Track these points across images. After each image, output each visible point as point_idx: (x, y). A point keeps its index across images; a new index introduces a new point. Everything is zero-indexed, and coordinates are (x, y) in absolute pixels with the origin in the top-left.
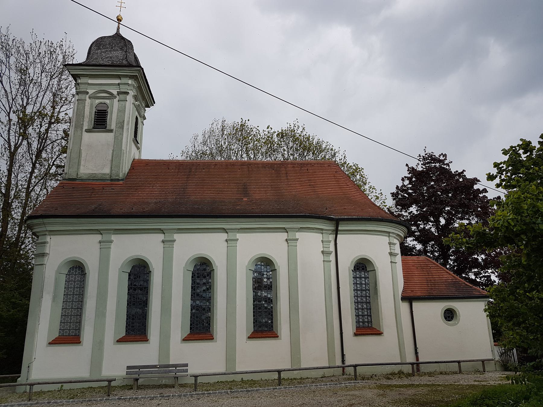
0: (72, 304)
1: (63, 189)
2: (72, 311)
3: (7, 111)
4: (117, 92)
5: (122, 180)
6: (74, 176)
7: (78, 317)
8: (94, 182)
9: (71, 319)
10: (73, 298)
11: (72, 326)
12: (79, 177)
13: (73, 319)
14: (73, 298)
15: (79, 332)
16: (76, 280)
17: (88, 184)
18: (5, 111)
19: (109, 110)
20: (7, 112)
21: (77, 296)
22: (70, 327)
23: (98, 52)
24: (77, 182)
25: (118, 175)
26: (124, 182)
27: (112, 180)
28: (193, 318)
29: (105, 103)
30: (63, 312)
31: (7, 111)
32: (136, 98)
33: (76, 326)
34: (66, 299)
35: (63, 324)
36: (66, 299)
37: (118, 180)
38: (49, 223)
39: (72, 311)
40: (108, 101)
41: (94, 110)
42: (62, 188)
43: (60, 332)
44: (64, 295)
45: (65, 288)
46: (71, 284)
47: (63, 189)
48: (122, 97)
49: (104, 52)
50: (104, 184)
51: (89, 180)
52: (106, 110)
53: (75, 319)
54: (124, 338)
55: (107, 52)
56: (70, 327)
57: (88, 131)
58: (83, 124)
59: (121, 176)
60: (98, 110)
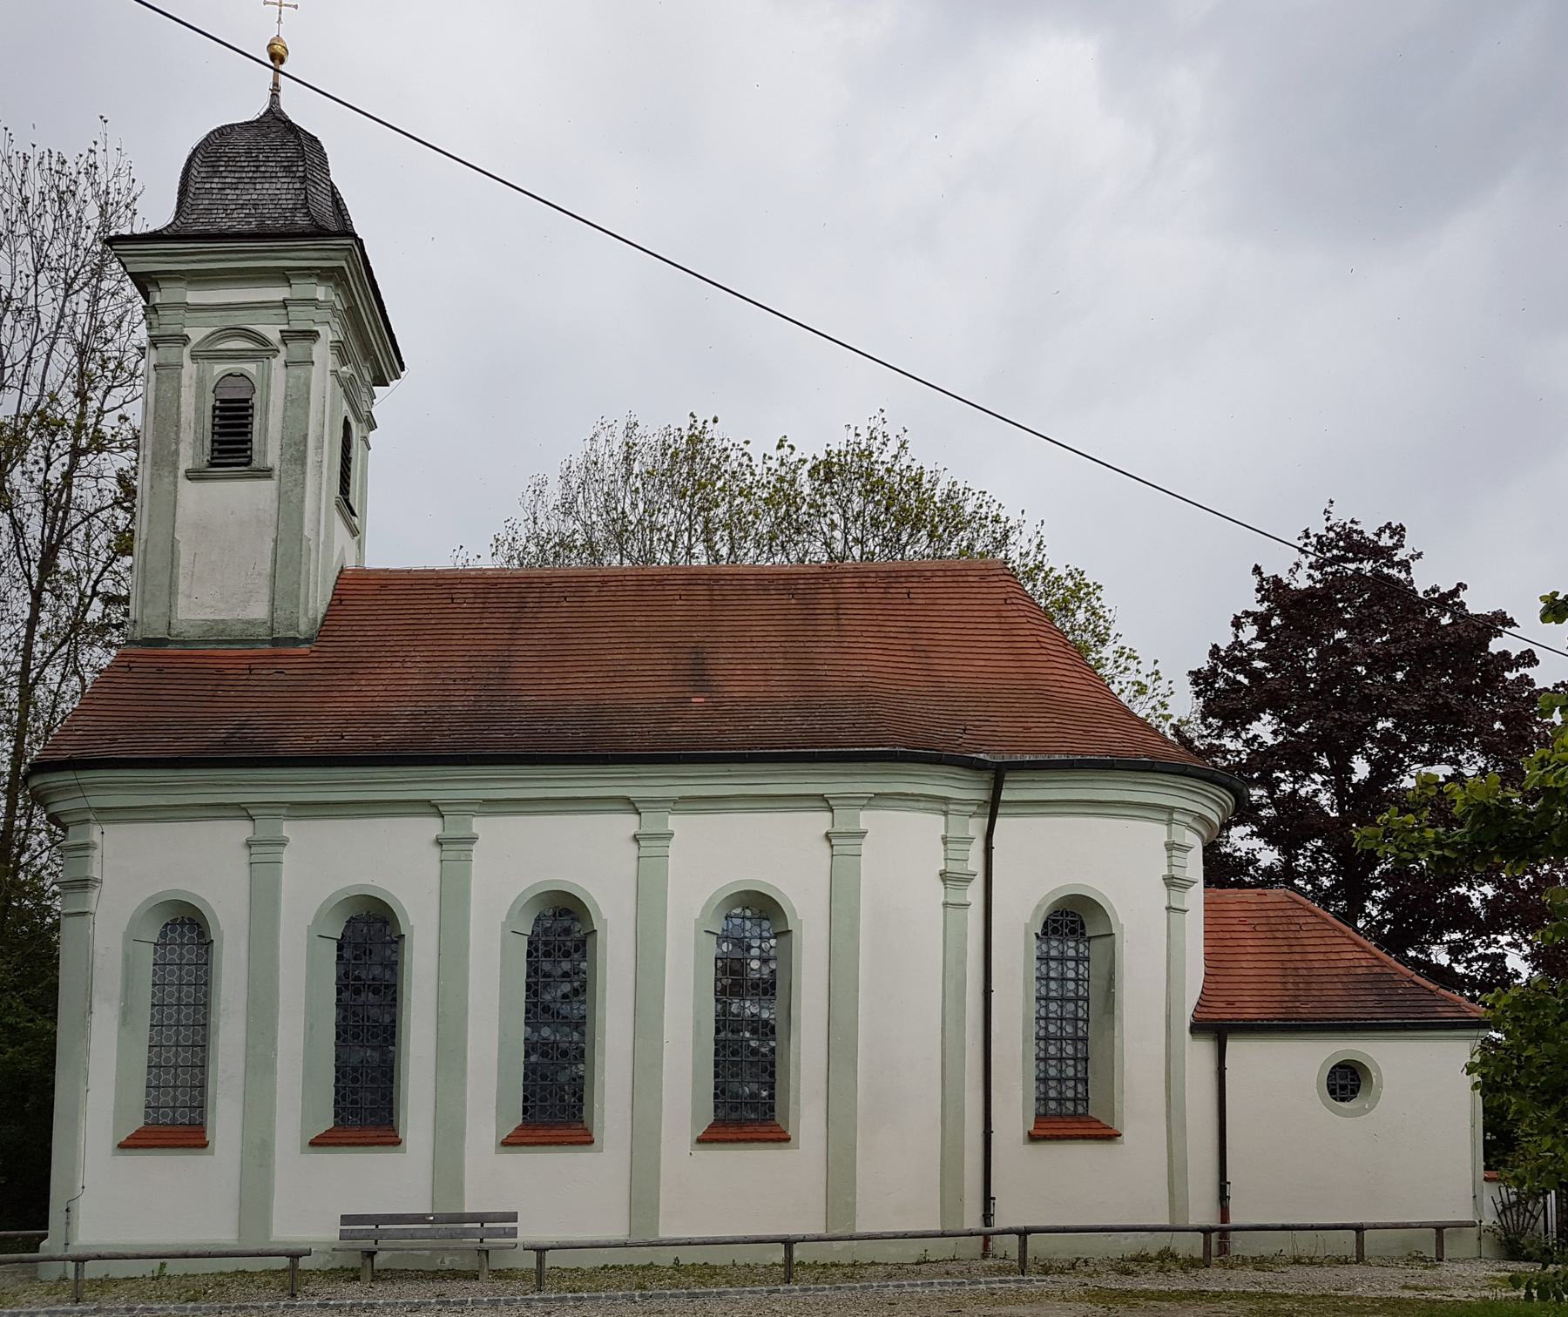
2: (177, 1054)
5: (307, 641)
6: (161, 633)
7: (197, 1071)
9: (176, 1076)
11: (181, 1098)
12: (174, 632)
19: (256, 400)
22: (175, 1099)
23: (214, 186)
24: (171, 650)
25: (296, 627)
26: (314, 649)
27: (275, 642)
29: (242, 375)
33: (192, 1099)
34: (157, 1017)
36: (157, 1017)
37: (295, 641)
40: (250, 368)
41: (210, 401)
43: (147, 1115)
44: (153, 1005)
45: (154, 985)
46: (171, 973)
48: (297, 348)
50: (253, 657)
51: (207, 642)
52: (246, 401)
53: (188, 1077)
54: (332, 1134)
55: (240, 186)
57: (194, 475)
59: (304, 628)
60: (222, 401)
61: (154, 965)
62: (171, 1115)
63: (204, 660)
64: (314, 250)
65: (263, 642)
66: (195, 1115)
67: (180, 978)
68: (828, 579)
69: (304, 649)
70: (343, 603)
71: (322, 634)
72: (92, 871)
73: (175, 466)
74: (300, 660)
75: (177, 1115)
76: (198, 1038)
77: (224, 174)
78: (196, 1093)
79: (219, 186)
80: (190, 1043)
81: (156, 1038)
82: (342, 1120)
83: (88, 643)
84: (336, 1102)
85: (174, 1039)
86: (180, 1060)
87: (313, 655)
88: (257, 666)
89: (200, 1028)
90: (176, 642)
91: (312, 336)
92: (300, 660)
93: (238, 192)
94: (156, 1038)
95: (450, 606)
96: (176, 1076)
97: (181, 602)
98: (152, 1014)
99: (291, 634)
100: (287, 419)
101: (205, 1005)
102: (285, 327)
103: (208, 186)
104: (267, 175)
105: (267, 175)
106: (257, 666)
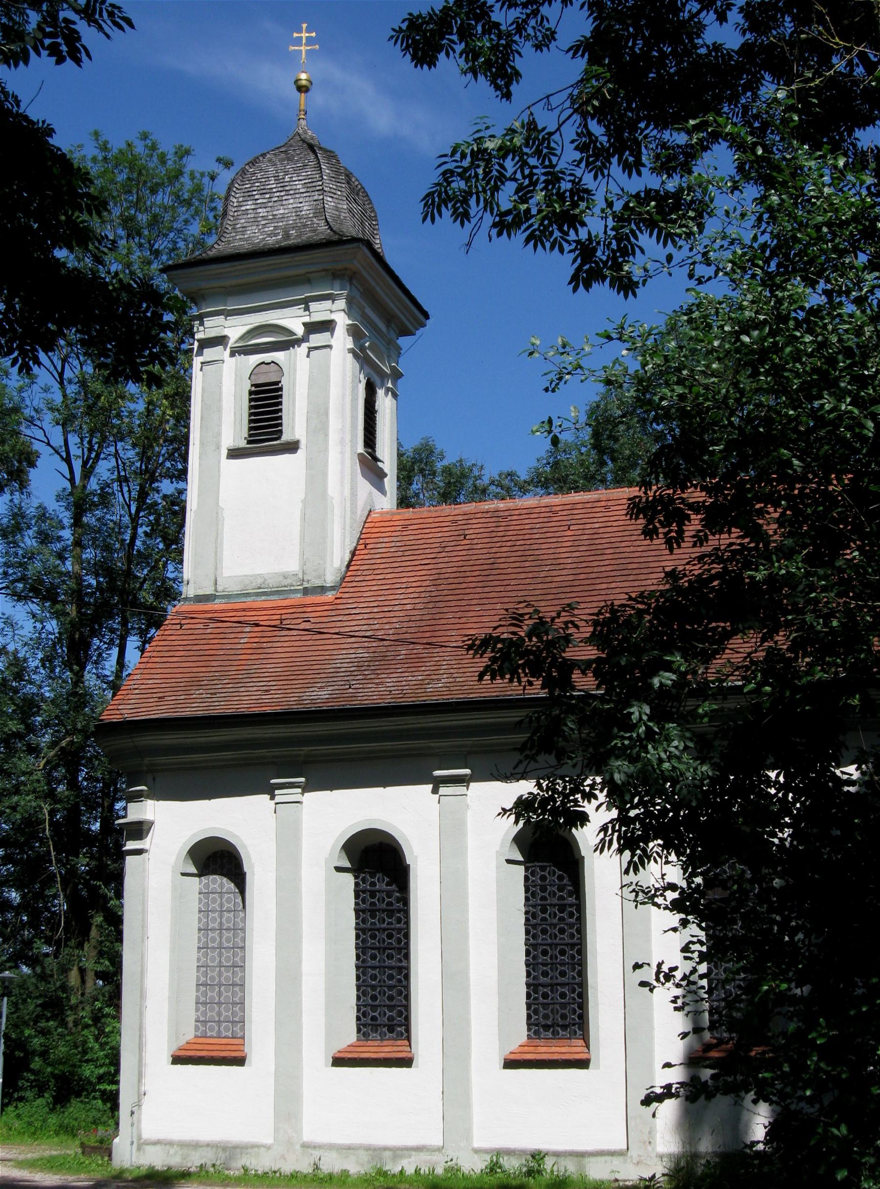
0: (220, 955)
1: (180, 632)
2: (220, 974)
3: (55, 368)
4: (304, 324)
5: (333, 588)
6: (209, 591)
7: (237, 989)
8: (261, 602)
9: (220, 994)
10: (221, 938)
11: (224, 1014)
12: (220, 588)
13: (225, 994)
14: (221, 938)
15: (243, 1029)
16: (224, 890)
17: (244, 610)
18: (52, 369)
19: (284, 382)
20: (57, 371)
21: (231, 935)
22: (219, 1014)
23: (248, 207)
24: (217, 605)
25: (322, 576)
26: (339, 595)
27: (306, 591)
28: (534, 999)
29: (273, 362)
30: (200, 974)
31: (55, 368)
32: (354, 332)
33: (234, 1014)
34: (203, 940)
35: (237, 980)
36: (203, 940)
37: (323, 589)
38: (342, 453)
39: (220, 974)
40: (279, 356)
41: (247, 386)
42: (178, 627)
43: (197, 1028)
44: (200, 930)
45: (200, 911)
46: (214, 901)
47: (180, 632)
48: (316, 339)
49: (264, 206)
50: (285, 608)
51: (248, 595)
52: (277, 383)
53: (230, 994)
54: (352, 1049)
55: (270, 204)
56: (219, 1014)
57: (235, 454)
58: (219, 434)
59: (330, 579)
60: (256, 386)
61: (200, 893)
62: (216, 1028)
63: (244, 613)
64: (255, 610)
65: (296, 591)
66: (237, 1029)
67: (221, 905)
68: (556, 512)
69: (330, 596)
70: (368, 547)
71: (347, 579)
72: (146, 813)
73: (218, 447)
74: (326, 608)
75: (222, 1028)
76: (237, 959)
77: (257, 197)
78: (237, 1009)
79: (253, 207)
80: (230, 964)
81: (203, 959)
82: (364, 1035)
83: (844, 292)
84: (358, 1018)
85: (218, 959)
86: (217, 1009)
87: (338, 601)
88: (288, 616)
89: (239, 950)
90: (223, 597)
91: (327, 326)
92: (326, 608)
93: (268, 209)
94: (203, 959)
95: (566, 533)
96: (220, 994)
97: (226, 563)
98: (199, 918)
99: (318, 583)
100: (247, 635)
101: (243, 948)
102: (307, 319)
103: (243, 208)
104: (292, 192)
105: (292, 192)
106: (288, 616)
